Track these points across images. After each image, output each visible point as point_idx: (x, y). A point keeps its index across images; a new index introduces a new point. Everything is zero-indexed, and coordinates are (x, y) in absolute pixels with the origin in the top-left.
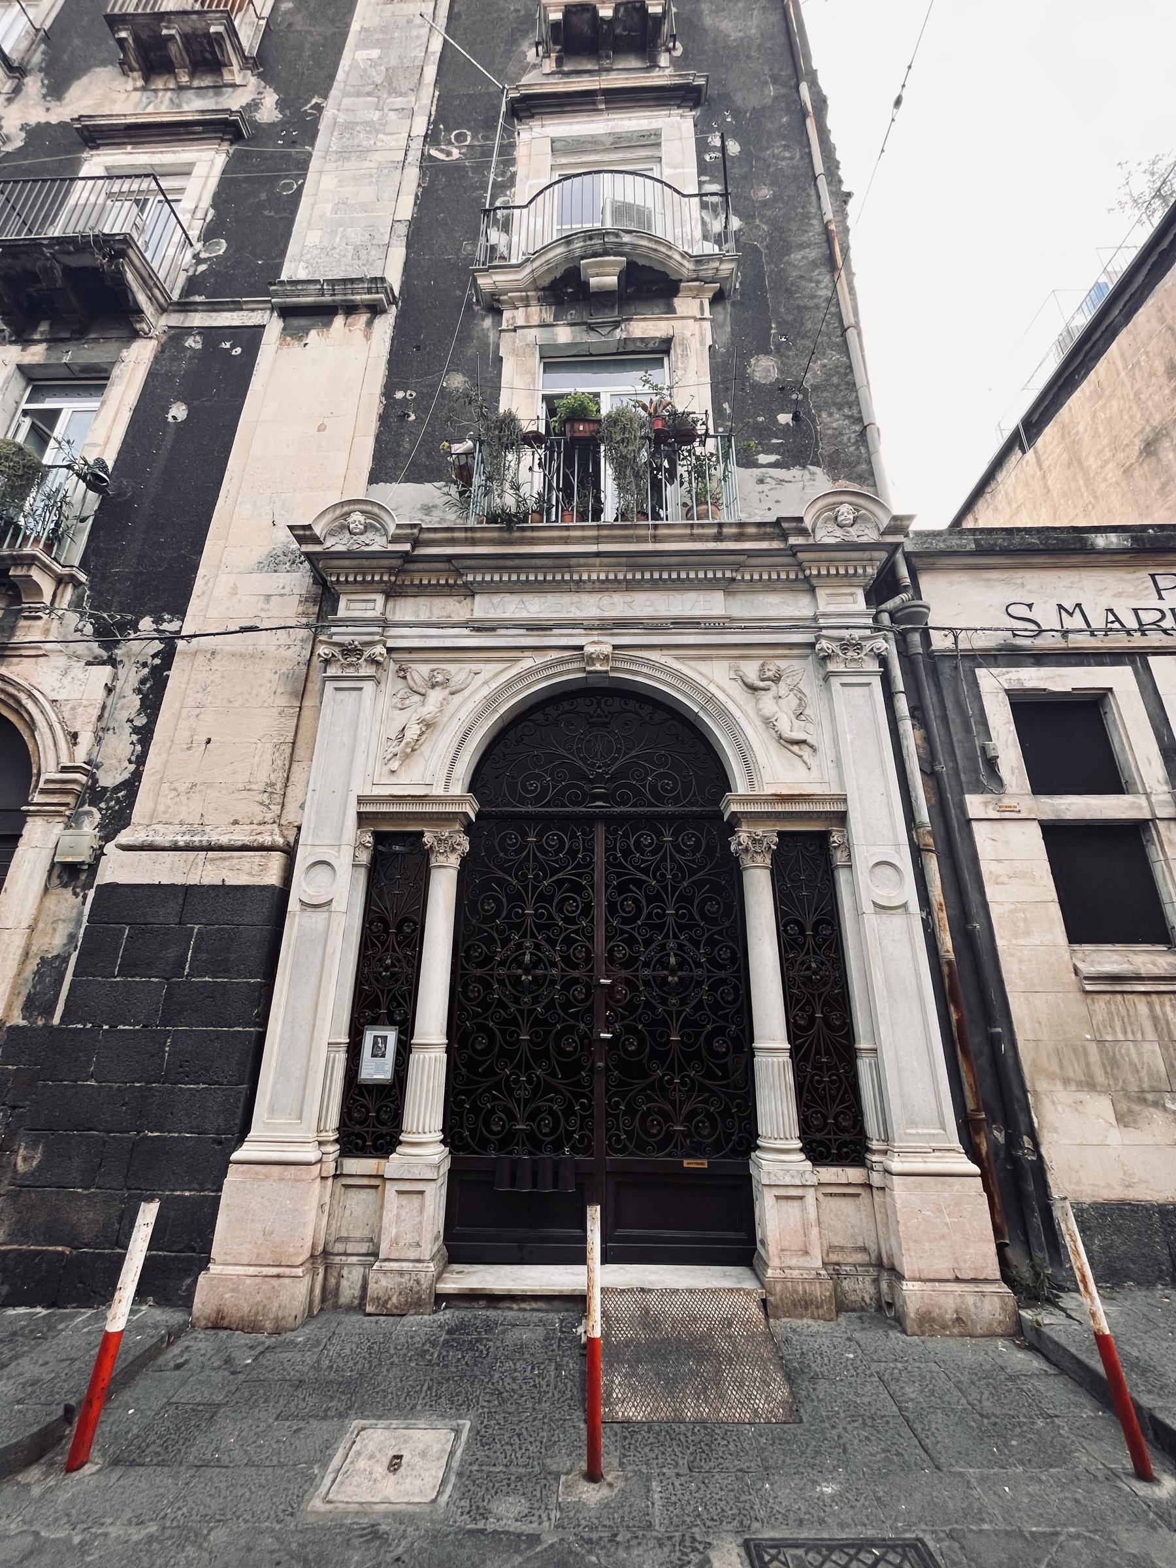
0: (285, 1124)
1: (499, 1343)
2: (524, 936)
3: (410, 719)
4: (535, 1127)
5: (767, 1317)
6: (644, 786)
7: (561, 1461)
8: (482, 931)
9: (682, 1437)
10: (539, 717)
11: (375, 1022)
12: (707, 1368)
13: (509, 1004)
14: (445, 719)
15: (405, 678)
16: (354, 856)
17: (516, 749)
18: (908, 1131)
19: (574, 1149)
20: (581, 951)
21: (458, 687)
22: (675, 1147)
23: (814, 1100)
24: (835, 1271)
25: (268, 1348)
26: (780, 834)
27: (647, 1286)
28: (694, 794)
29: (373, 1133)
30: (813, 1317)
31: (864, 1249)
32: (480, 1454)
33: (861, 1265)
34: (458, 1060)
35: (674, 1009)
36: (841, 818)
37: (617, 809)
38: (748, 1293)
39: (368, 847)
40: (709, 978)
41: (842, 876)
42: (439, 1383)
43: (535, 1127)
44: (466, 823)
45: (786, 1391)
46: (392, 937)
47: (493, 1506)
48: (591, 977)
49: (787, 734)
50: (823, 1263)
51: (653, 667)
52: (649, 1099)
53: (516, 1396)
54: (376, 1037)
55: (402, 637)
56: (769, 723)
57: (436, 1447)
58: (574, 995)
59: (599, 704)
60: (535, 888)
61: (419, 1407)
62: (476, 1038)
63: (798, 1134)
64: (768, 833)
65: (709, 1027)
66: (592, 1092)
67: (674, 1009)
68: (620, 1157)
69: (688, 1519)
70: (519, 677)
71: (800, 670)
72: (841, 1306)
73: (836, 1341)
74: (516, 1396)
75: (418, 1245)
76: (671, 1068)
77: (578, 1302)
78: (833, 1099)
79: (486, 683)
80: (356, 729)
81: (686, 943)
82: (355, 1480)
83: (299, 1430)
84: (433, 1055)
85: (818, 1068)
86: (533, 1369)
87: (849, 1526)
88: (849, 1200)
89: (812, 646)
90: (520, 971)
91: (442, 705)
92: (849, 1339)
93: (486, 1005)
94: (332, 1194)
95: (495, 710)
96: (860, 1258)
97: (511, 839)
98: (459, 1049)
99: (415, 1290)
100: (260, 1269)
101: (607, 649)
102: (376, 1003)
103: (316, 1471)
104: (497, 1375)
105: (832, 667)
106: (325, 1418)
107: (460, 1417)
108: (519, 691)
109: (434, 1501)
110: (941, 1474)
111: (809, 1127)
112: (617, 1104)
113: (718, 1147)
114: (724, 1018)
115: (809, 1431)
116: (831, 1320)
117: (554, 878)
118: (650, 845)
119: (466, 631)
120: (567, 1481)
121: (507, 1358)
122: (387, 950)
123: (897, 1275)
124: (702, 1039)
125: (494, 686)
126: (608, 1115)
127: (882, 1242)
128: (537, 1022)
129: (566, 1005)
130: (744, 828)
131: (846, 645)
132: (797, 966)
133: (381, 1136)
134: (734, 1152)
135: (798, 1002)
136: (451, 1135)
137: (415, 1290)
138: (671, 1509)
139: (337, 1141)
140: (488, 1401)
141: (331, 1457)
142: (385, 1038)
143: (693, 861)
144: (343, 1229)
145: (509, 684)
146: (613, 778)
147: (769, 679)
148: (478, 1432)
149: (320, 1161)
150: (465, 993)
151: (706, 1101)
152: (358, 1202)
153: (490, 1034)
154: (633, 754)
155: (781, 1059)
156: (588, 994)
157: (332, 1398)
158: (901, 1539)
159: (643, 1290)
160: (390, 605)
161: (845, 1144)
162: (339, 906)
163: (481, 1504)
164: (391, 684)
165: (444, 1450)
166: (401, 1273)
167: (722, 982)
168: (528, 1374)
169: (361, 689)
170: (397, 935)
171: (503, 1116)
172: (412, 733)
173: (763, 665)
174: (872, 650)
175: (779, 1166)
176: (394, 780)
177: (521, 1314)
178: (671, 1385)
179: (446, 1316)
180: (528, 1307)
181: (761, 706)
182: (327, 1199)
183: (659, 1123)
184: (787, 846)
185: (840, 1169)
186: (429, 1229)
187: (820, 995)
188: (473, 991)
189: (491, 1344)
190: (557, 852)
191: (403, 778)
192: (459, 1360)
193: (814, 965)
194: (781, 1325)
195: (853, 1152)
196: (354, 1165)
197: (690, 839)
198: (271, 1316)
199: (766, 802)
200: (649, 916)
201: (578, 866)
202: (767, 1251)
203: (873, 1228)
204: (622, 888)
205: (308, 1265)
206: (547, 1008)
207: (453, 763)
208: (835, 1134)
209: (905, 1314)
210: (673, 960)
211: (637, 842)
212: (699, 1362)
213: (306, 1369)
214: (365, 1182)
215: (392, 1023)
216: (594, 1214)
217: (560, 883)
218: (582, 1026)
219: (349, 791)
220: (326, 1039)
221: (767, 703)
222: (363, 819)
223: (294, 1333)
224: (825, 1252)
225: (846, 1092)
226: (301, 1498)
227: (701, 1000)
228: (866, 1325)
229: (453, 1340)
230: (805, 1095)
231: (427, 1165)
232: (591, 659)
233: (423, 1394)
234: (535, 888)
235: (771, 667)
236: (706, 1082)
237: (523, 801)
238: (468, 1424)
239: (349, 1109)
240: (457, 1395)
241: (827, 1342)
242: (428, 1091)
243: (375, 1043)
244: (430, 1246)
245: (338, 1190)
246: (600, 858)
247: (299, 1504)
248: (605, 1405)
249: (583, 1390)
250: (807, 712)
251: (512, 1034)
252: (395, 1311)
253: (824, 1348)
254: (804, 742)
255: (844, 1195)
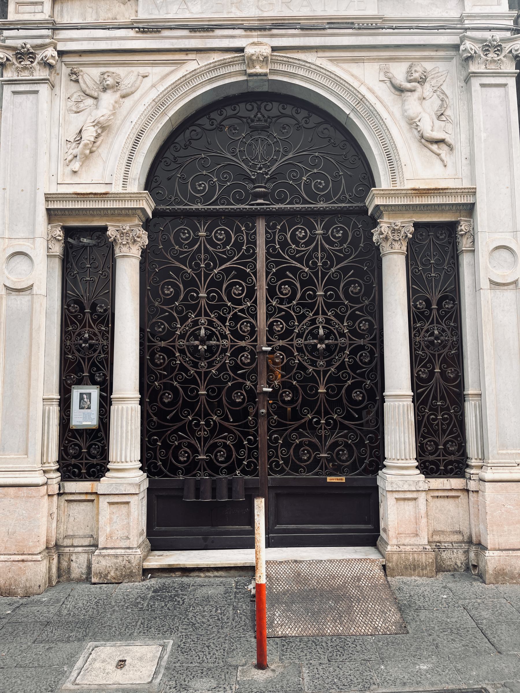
0: (15, 459)
1: (191, 597)
2: (199, 315)
3: (86, 120)
4: (213, 457)
5: (386, 575)
6: (299, 185)
7: (238, 659)
8: (164, 311)
9: (324, 644)
10: (204, 121)
11: (80, 382)
12: (342, 606)
13: (189, 368)
14: (118, 122)
15: (77, 81)
16: (49, 248)
17: (186, 145)
18: (501, 452)
19: (243, 472)
20: (246, 326)
21: (129, 91)
22: (321, 468)
23: (429, 433)
24: (438, 547)
25: (22, 604)
26: (416, 225)
27: (298, 559)
28: (343, 192)
29: (86, 464)
30: (419, 576)
31: (460, 532)
32: (181, 658)
33: (457, 543)
34: (150, 411)
35: (322, 369)
36: (470, 209)
37: (277, 206)
38: (373, 561)
39: (59, 240)
40: (350, 345)
41: (465, 260)
42: (149, 620)
43: (213, 457)
44: (144, 219)
45: (398, 616)
46: (88, 316)
47: (192, 684)
48: (255, 346)
49: (429, 133)
50: (428, 542)
51: (309, 69)
52: (301, 435)
53: (205, 625)
54: (81, 394)
55: (72, 40)
56: (412, 123)
57: (149, 655)
58: (241, 360)
59: (259, 109)
60: (207, 276)
61: (135, 634)
62: (164, 394)
63: (415, 457)
64: (406, 224)
65: (349, 382)
66: (257, 431)
67: (322, 369)
68: (278, 476)
69: (327, 686)
70: (185, 80)
71: (443, 72)
72: (440, 568)
73: (434, 589)
74: (205, 625)
75: (128, 538)
76: (318, 413)
77: (250, 570)
78: (444, 431)
79: (153, 86)
80: (37, 131)
81: (332, 318)
82: (94, 673)
83: (51, 648)
84: (129, 406)
85: (434, 409)
86: (217, 610)
87: (437, 684)
88: (451, 500)
89: (456, 47)
90: (197, 343)
91: (114, 107)
92: (445, 587)
93: (170, 369)
94: (58, 507)
95: (164, 113)
96: (456, 538)
97: (184, 234)
98: (150, 403)
99: (127, 567)
100: (9, 557)
101: (266, 51)
102: (79, 369)
103: (66, 669)
104: (191, 615)
105: (473, 68)
106: (68, 641)
107: (165, 638)
108: (186, 94)
109: (151, 682)
110: (502, 656)
111: (424, 452)
112: (277, 439)
113: (353, 468)
114: (362, 375)
115: (413, 638)
116: (432, 577)
117: (223, 267)
118: (304, 237)
119: (131, 33)
120: (243, 669)
121: (198, 604)
122: (84, 326)
123: (481, 547)
124: (343, 391)
125: (161, 88)
126: (269, 447)
127: (473, 526)
128: (212, 381)
129: (236, 368)
130: (385, 219)
131: (488, 47)
132: (422, 333)
133: (93, 466)
134: (366, 471)
135: (421, 360)
136: (148, 464)
137: (127, 567)
138: (315, 681)
139: (58, 470)
140: (185, 629)
141: (75, 662)
142: (90, 394)
143: (340, 251)
144: (69, 530)
145: (175, 87)
146: (272, 178)
147: (415, 80)
148: (179, 646)
149: (46, 484)
150: (152, 360)
151: (345, 436)
152: (79, 513)
153: (175, 390)
154: (290, 155)
155: (405, 403)
156: (253, 359)
157: (72, 631)
158: (471, 689)
159: (296, 561)
160: (57, 7)
161: (451, 463)
162: (40, 289)
163: (183, 683)
164: (65, 87)
165: (154, 656)
166: (116, 556)
167: (361, 348)
168: (213, 613)
169: (36, 92)
170: (91, 314)
171: (188, 450)
172: (89, 134)
173: (411, 67)
174: (511, 52)
175: (400, 478)
176: (76, 180)
177: (207, 580)
178: (315, 615)
179: (153, 582)
180: (212, 575)
181: (406, 107)
182: (55, 510)
183: (309, 452)
184: (421, 235)
185: (445, 480)
186: (135, 527)
187: (439, 355)
188: (159, 359)
189: (186, 597)
190: (225, 245)
191: (83, 178)
192: (163, 607)
193: (436, 332)
194: (395, 581)
195: (456, 468)
196: (71, 486)
197: (338, 232)
198: (21, 586)
199: (406, 195)
200: (302, 297)
201: (243, 257)
202: (388, 535)
203: (467, 518)
204: (280, 274)
205: (45, 553)
206: (219, 370)
207: (129, 164)
208: (444, 456)
209: (485, 571)
210: (321, 332)
211: (293, 235)
212: (336, 602)
213: (51, 616)
214: (83, 497)
215: (94, 383)
216: (260, 506)
217: (227, 271)
218: (248, 383)
219: (36, 189)
220: (41, 396)
221: (412, 104)
222: (52, 215)
223: (40, 596)
224: (430, 532)
225: (454, 426)
226: (56, 683)
227: (343, 362)
228: (457, 579)
229: (158, 596)
230: (422, 429)
231: (130, 484)
232: (251, 61)
233: (138, 627)
234: (207, 276)
235: (418, 68)
236: (346, 422)
237: (193, 200)
238: (171, 642)
239: (66, 448)
240: (162, 626)
241: (429, 590)
242: (127, 432)
243: (81, 398)
244: (136, 538)
245: (62, 504)
246: (261, 250)
247: (56, 686)
248: (269, 628)
249: (253, 620)
250: (448, 112)
251: (192, 390)
252: (114, 581)
253: (426, 593)
254: (442, 141)
255: (447, 497)
